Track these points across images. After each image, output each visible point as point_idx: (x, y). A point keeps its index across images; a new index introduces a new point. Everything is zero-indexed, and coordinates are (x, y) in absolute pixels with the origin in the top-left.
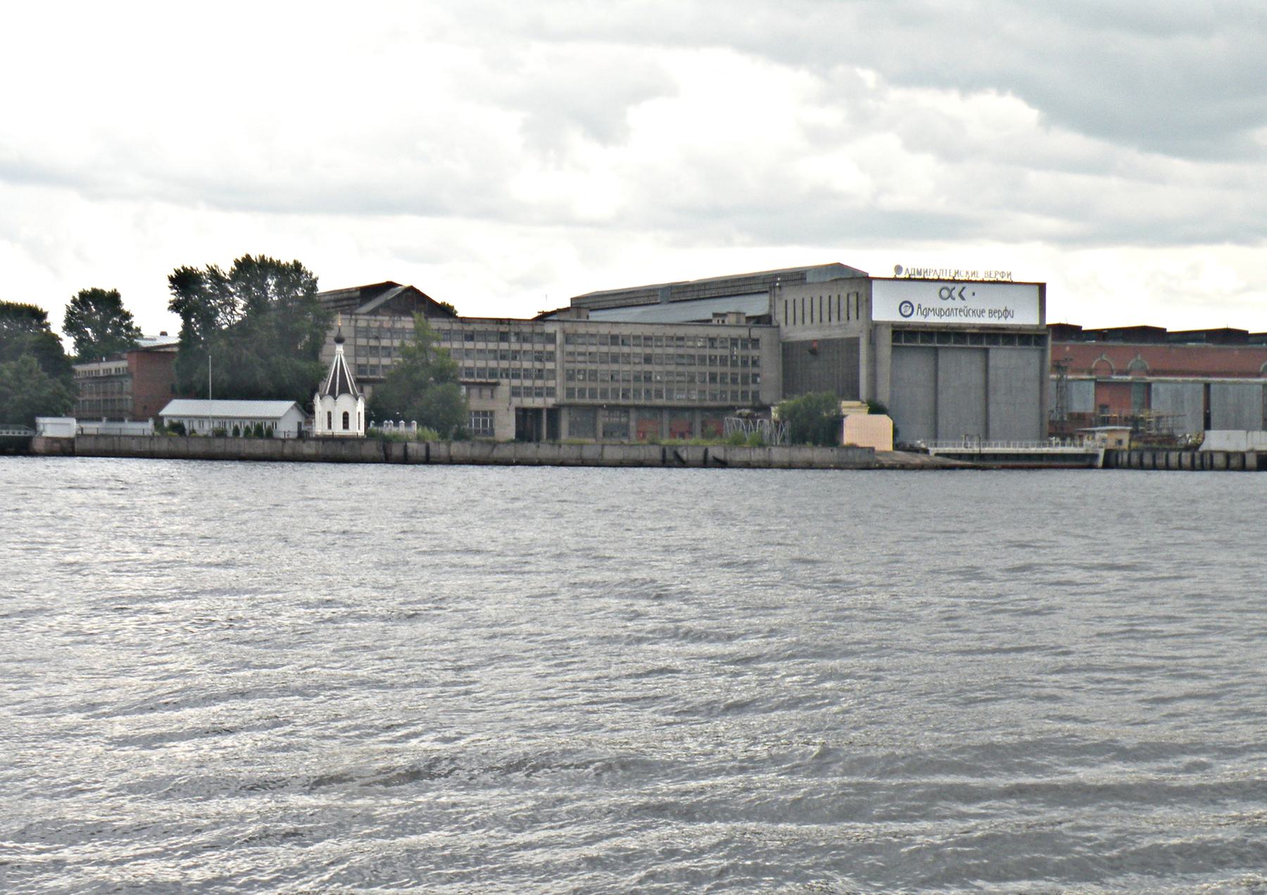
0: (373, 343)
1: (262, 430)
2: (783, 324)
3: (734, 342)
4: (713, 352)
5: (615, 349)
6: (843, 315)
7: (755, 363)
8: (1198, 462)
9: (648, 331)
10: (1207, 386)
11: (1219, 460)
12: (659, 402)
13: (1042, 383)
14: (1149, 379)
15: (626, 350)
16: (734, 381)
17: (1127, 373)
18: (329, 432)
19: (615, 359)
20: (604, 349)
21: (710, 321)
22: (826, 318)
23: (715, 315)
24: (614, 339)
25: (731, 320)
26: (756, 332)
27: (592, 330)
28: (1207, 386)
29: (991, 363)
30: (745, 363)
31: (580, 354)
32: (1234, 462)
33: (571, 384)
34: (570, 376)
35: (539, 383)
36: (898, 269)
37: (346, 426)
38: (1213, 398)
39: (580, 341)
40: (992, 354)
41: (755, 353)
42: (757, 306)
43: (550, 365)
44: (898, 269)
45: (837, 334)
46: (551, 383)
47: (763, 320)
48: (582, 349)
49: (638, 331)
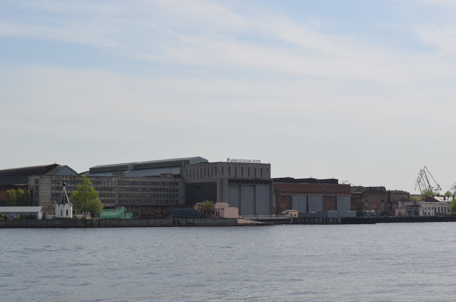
0: (57, 185)
1: (33, 216)
2: (186, 178)
3: (170, 183)
4: (164, 187)
5: (134, 186)
6: (210, 174)
7: (177, 191)
8: (325, 221)
9: (144, 180)
10: (307, 197)
11: (331, 220)
12: (147, 204)
13: (270, 196)
14: (291, 195)
15: (137, 186)
16: (170, 197)
17: (285, 193)
18: (61, 217)
19: (134, 189)
20: (131, 186)
21: (160, 176)
22: (203, 175)
23: (162, 174)
24: (134, 183)
25: (168, 176)
26: (177, 180)
27: (127, 180)
28: (307, 197)
29: (256, 190)
30: (174, 191)
31: (123, 188)
32: (335, 221)
33: (120, 199)
34: (120, 196)
35: (110, 198)
36: (228, 159)
37: (67, 214)
38: (309, 201)
39: (123, 184)
40: (256, 187)
41: (177, 187)
42: (176, 171)
43: (113, 192)
44: (228, 159)
45: (208, 181)
46: (114, 198)
47: (179, 176)
48: (123, 186)
49: (142, 180)
